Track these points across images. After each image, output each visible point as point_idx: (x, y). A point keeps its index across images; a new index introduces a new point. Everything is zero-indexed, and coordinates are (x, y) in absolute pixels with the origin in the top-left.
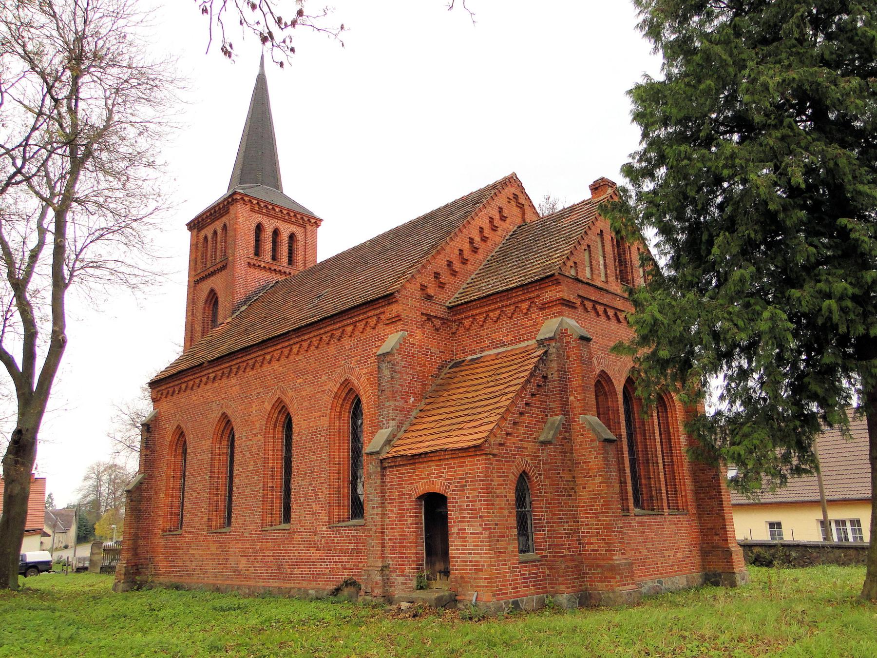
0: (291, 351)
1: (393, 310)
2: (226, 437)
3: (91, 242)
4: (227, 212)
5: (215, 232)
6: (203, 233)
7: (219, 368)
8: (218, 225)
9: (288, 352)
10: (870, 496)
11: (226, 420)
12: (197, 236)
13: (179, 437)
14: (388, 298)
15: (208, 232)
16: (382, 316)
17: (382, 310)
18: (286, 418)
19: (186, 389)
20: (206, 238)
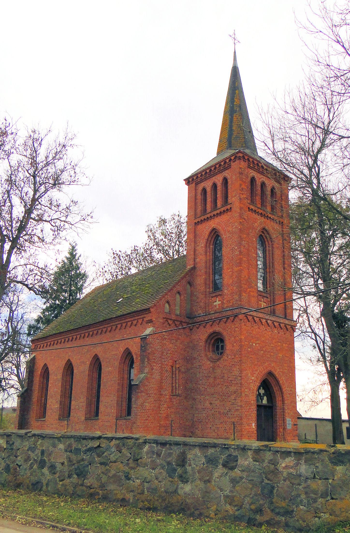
0: (126, 325)
1: (148, 317)
2: (127, 361)
3: (340, 38)
4: (229, 167)
5: (215, 186)
6: (200, 187)
7: (41, 343)
8: (218, 179)
9: (141, 321)
10: (330, 417)
11: (69, 363)
12: (196, 190)
13: (96, 361)
14: (147, 311)
15: (208, 184)
16: (144, 319)
17: (145, 315)
18: (98, 365)
19: (97, 334)
20: (204, 191)
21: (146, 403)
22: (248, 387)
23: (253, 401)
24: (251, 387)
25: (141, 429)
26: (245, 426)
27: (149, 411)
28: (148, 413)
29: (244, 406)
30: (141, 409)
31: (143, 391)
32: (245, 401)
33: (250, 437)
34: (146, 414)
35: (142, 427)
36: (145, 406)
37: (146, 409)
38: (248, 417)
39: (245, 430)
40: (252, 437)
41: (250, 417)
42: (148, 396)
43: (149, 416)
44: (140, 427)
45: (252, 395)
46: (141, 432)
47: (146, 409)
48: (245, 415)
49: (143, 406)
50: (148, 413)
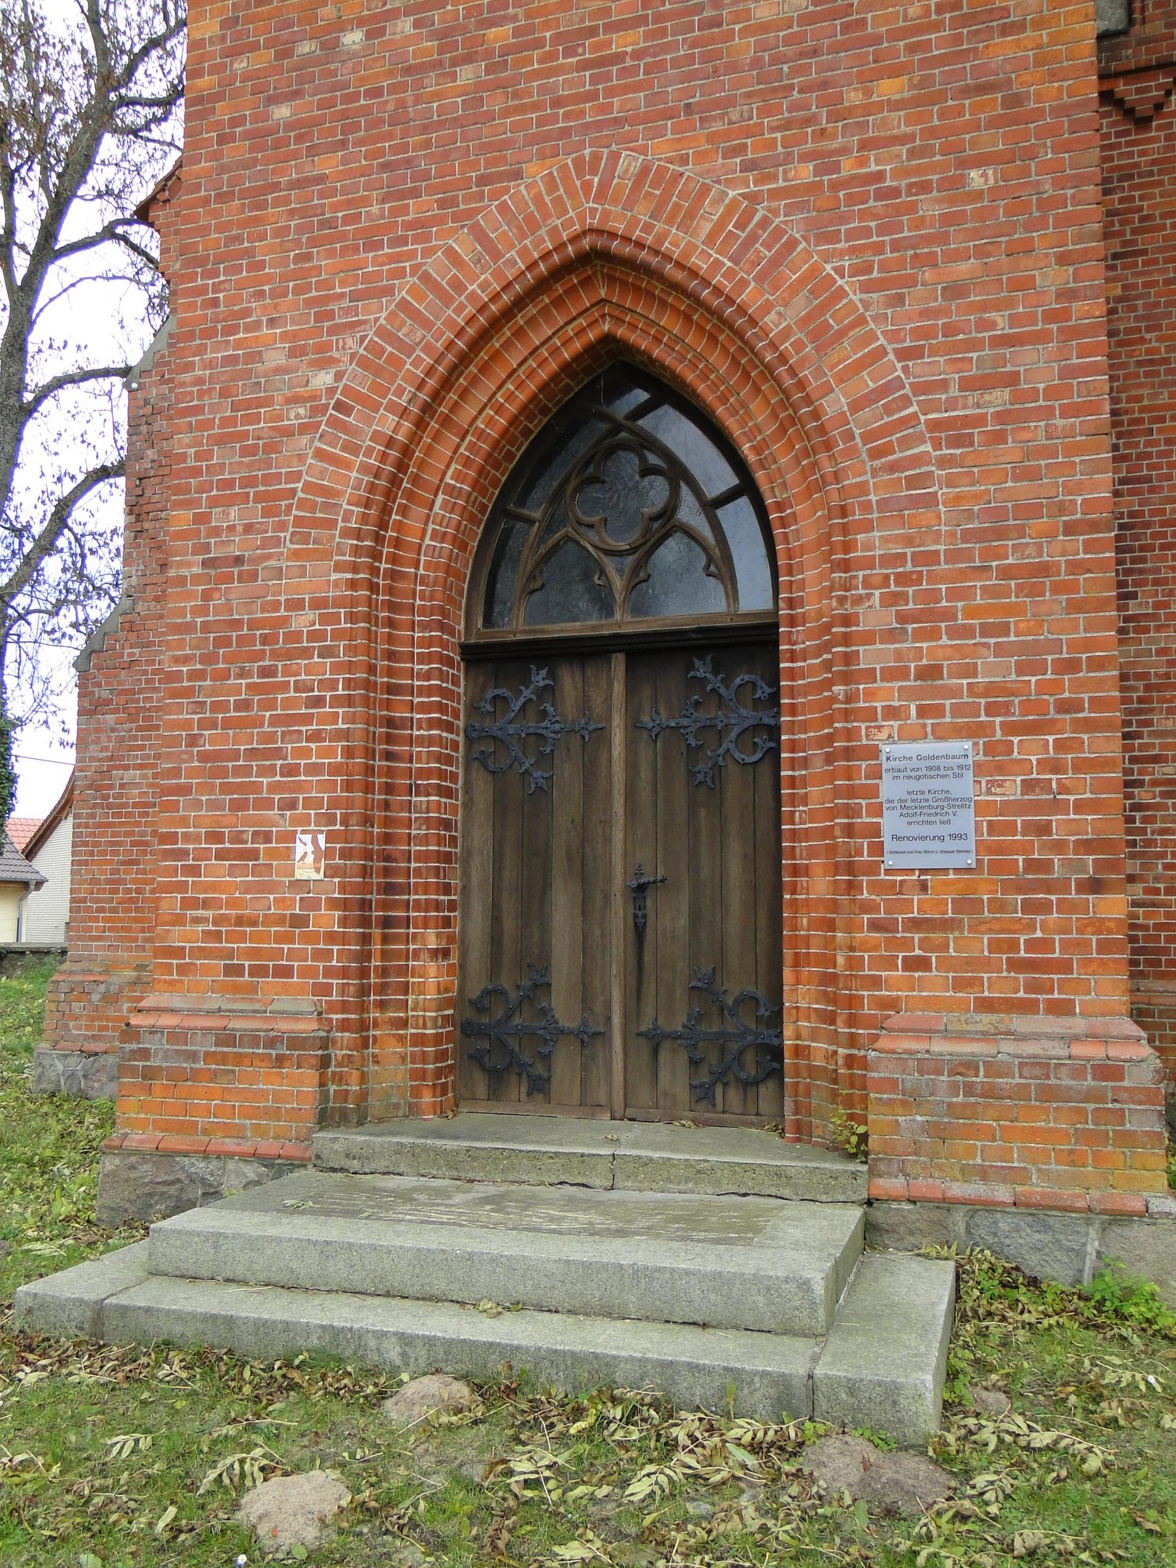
21: (126, 768)
22: (250, 482)
23: (317, 604)
24: (295, 476)
25: (96, 919)
26: (194, 871)
27: (146, 814)
28: (138, 824)
29: (195, 675)
30: (95, 806)
31: (108, 702)
32: (206, 627)
33: (257, 971)
34: (127, 834)
35: (101, 910)
36: (122, 786)
37: (125, 805)
38: (246, 771)
39: (188, 904)
40: (286, 972)
41: (263, 772)
42: (139, 729)
43: (146, 843)
44: (89, 909)
45: (297, 555)
46: (100, 938)
47: (125, 805)
48: (204, 757)
49: (111, 787)
50: (138, 824)
